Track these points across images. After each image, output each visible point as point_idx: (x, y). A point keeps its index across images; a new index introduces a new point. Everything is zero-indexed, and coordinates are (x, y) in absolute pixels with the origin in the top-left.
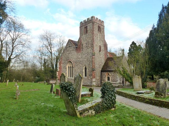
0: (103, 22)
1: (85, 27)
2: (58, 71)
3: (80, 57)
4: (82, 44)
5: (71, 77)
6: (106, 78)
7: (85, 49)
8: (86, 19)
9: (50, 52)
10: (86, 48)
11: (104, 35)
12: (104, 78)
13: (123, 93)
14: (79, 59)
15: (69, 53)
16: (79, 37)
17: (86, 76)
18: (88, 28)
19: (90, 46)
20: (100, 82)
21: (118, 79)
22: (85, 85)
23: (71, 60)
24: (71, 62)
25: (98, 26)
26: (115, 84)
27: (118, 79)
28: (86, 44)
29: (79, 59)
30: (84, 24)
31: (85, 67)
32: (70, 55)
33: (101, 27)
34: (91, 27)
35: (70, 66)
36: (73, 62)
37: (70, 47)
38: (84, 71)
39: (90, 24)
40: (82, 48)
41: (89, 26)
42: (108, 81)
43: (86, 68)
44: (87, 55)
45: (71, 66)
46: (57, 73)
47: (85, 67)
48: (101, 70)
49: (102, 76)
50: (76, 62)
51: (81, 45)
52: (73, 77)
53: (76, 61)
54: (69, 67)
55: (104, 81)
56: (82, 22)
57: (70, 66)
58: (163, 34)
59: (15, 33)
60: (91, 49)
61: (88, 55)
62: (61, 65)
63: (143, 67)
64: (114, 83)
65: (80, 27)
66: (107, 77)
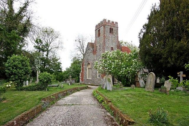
0: (117, 23)
11: (118, 37)
25: (110, 28)
28: (99, 46)
33: (114, 29)
39: (102, 27)
41: (102, 29)
46: (80, 74)
59: (48, 38)
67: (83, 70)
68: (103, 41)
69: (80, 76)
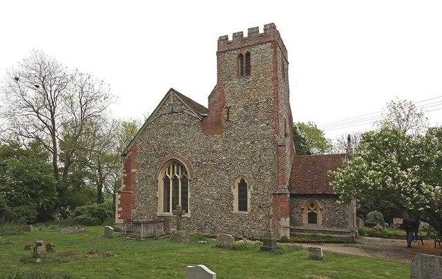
1: (241, 56)
3: (218, 147)
4: (228, 108)
9: (48, 127)
13: (387, 238)
14: (213, 156)
16: (215, 83)
17: (243, 206)
19: (261, 114)
21: (347, 220)
22: (320, 195)
24: (179, 164)
26: (336, 232)
28: (246, 108)
29: (213, 156)
34: (253, 59)
36: (187, 162)
38: (235, 192)
42: (312, 227)
43: (243, 187)
51: (225, 110)
54: (166, 180)
56: (226, 37)
58: (260, 221)
61: (253, 143)
65: (218, 53)
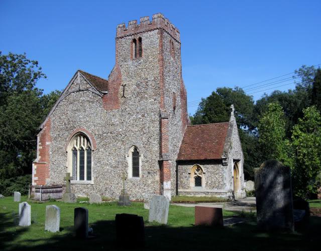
1: (134, 41)
2: (36, 163)
3: (115, 120)
5: (82, 178)
6: (190, 179)
7: (132, 103)
8: (209, 94)
10: (138, 98)
12: (184, 180)
14: (112, 128)
15: (75, 108)
17: (136, 173)
18: (143, 42)
19: (150, 91)
20: (175, 191)
23: (84, 130)
24: (85, 137)
27: (225, 182)
28: (138, 85)
29: (112, 128)
30: (133, 32)
31: (136, 149)
32: (81, 115)
35: (78, 148)
36: (91, 135)
37: (80, 91)
38: (130, 160)
39: (152, 32)
40: (123, 96)
42: (198, 189)
43: (136, 155)
44: (140, 116)
45: (84, 148)
46: (34, 167)
47: (133, 151)
48: (176, 157)
49: (179, 174)
50: (100, 136)
51: (121, 87)
52: (89, 178)
53: (101, 133)
54: (75, 151)
55: (183, 187)
57: (78, 148)
60: (155, 100)
61: (143, 116)
62: (47, 143)
63: (12, 171)
64: (215, 190)
66: (193, 176)
67: (43, 154)
68: (157, 71)
69: (34, 172)
